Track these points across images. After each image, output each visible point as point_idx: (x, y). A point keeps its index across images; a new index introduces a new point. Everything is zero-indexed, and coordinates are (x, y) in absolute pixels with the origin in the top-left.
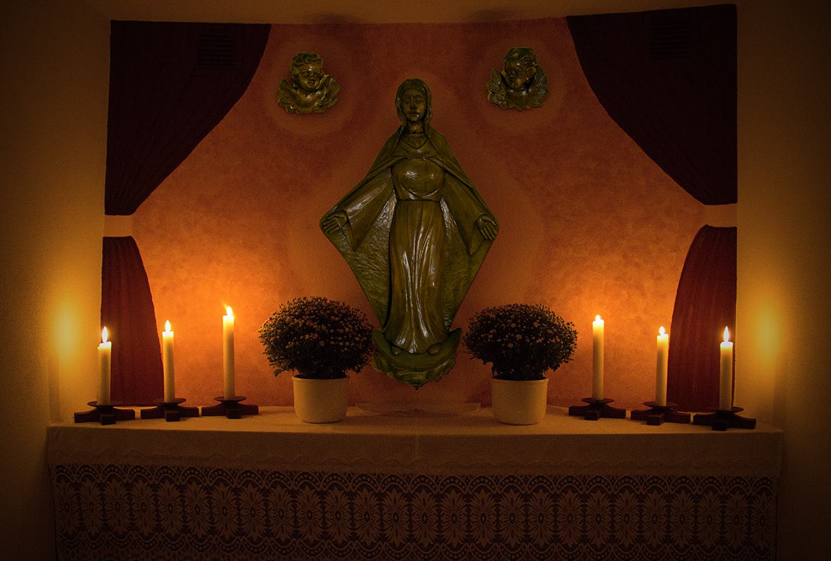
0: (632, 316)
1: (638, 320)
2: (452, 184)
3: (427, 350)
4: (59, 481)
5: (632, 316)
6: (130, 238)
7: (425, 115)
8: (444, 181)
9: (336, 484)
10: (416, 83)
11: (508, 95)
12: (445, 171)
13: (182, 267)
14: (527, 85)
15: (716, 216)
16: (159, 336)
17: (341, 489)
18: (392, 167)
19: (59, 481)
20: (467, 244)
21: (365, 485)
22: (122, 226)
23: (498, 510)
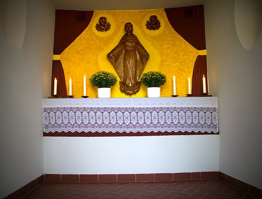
0: (183, 77)
1: (184, 78)
2: (138, 46)
3: (133, 86)
4: (44, 112)
5: (183, 77)
6: (59, 61)
7: (131, 31)
8: (136, 46)
9: (133, 110)
10: (130, 23)
11: (151, 26)
12: (136, 43)
13: (72, 67)
14: (155, 24)
15: (203, 53)
16: (66, 84)
17: (135, 111)
18: (124, 42)
19: (44, 112)
20: (142, 61)
21: (140, 110)
22: (57, 57)
23: (185, 116)
